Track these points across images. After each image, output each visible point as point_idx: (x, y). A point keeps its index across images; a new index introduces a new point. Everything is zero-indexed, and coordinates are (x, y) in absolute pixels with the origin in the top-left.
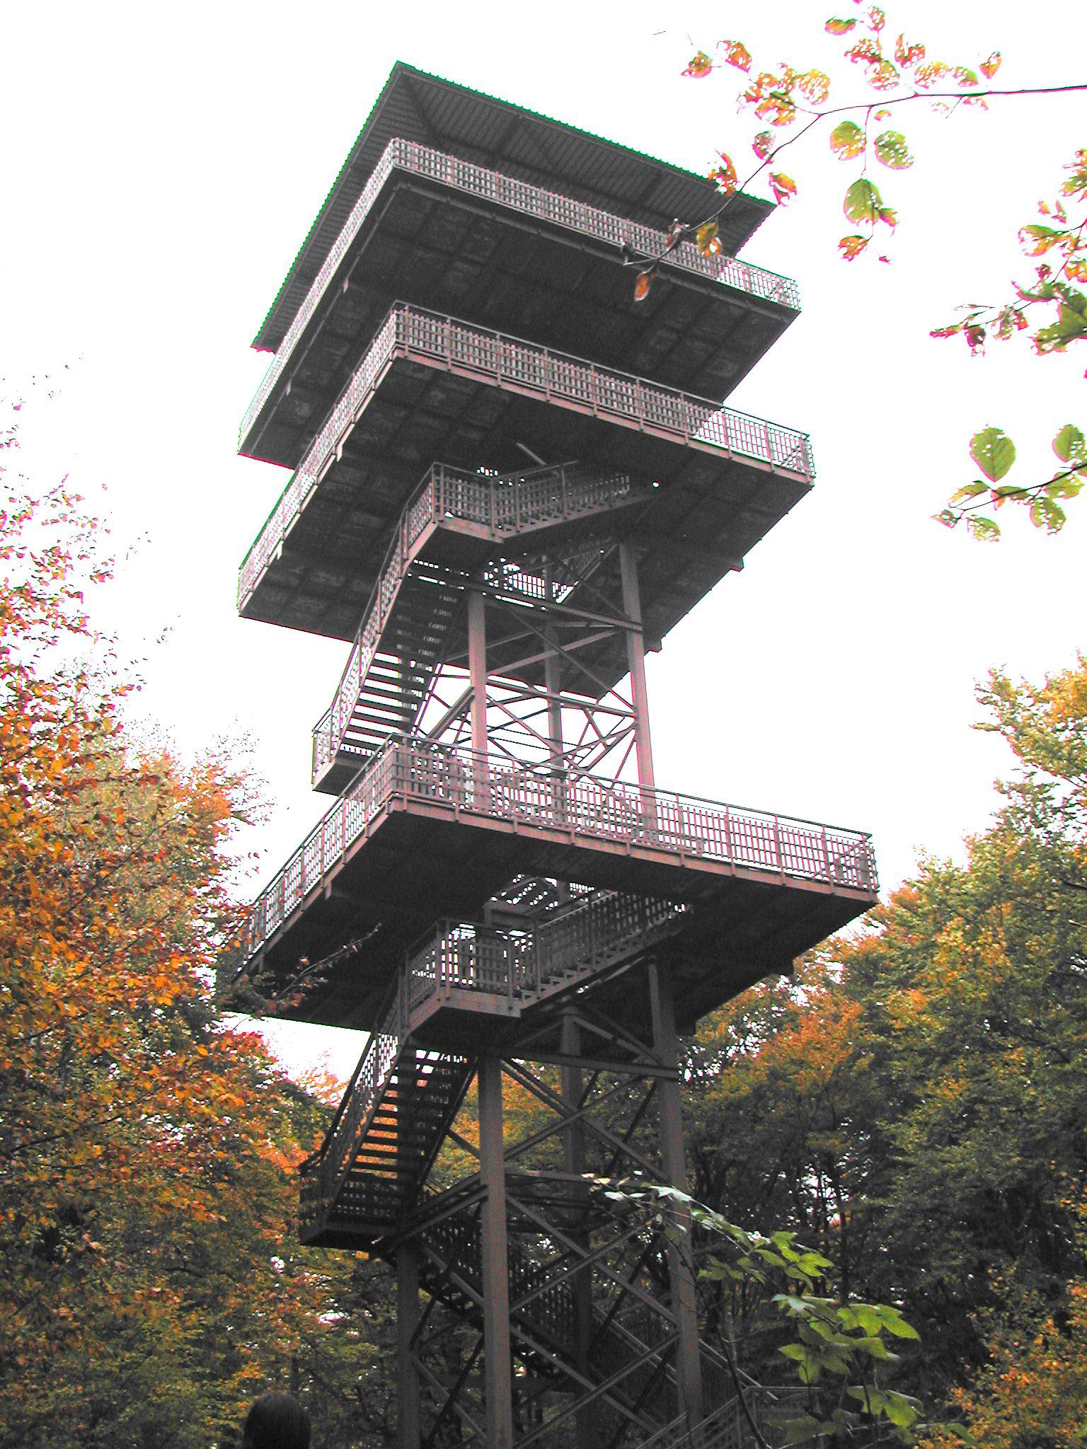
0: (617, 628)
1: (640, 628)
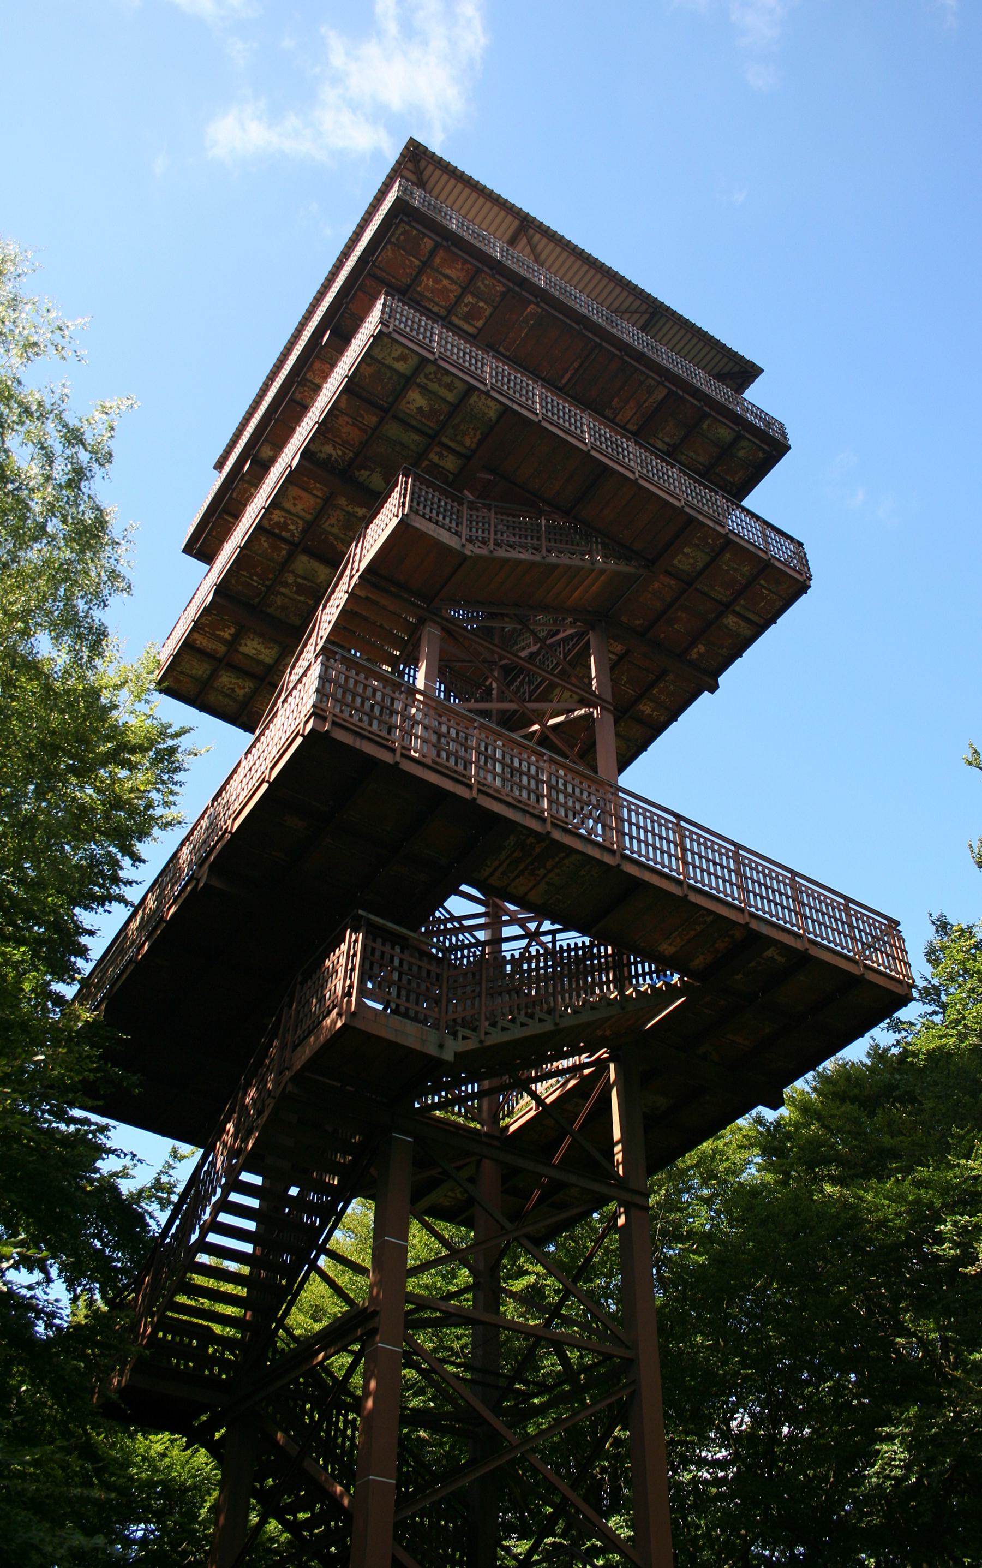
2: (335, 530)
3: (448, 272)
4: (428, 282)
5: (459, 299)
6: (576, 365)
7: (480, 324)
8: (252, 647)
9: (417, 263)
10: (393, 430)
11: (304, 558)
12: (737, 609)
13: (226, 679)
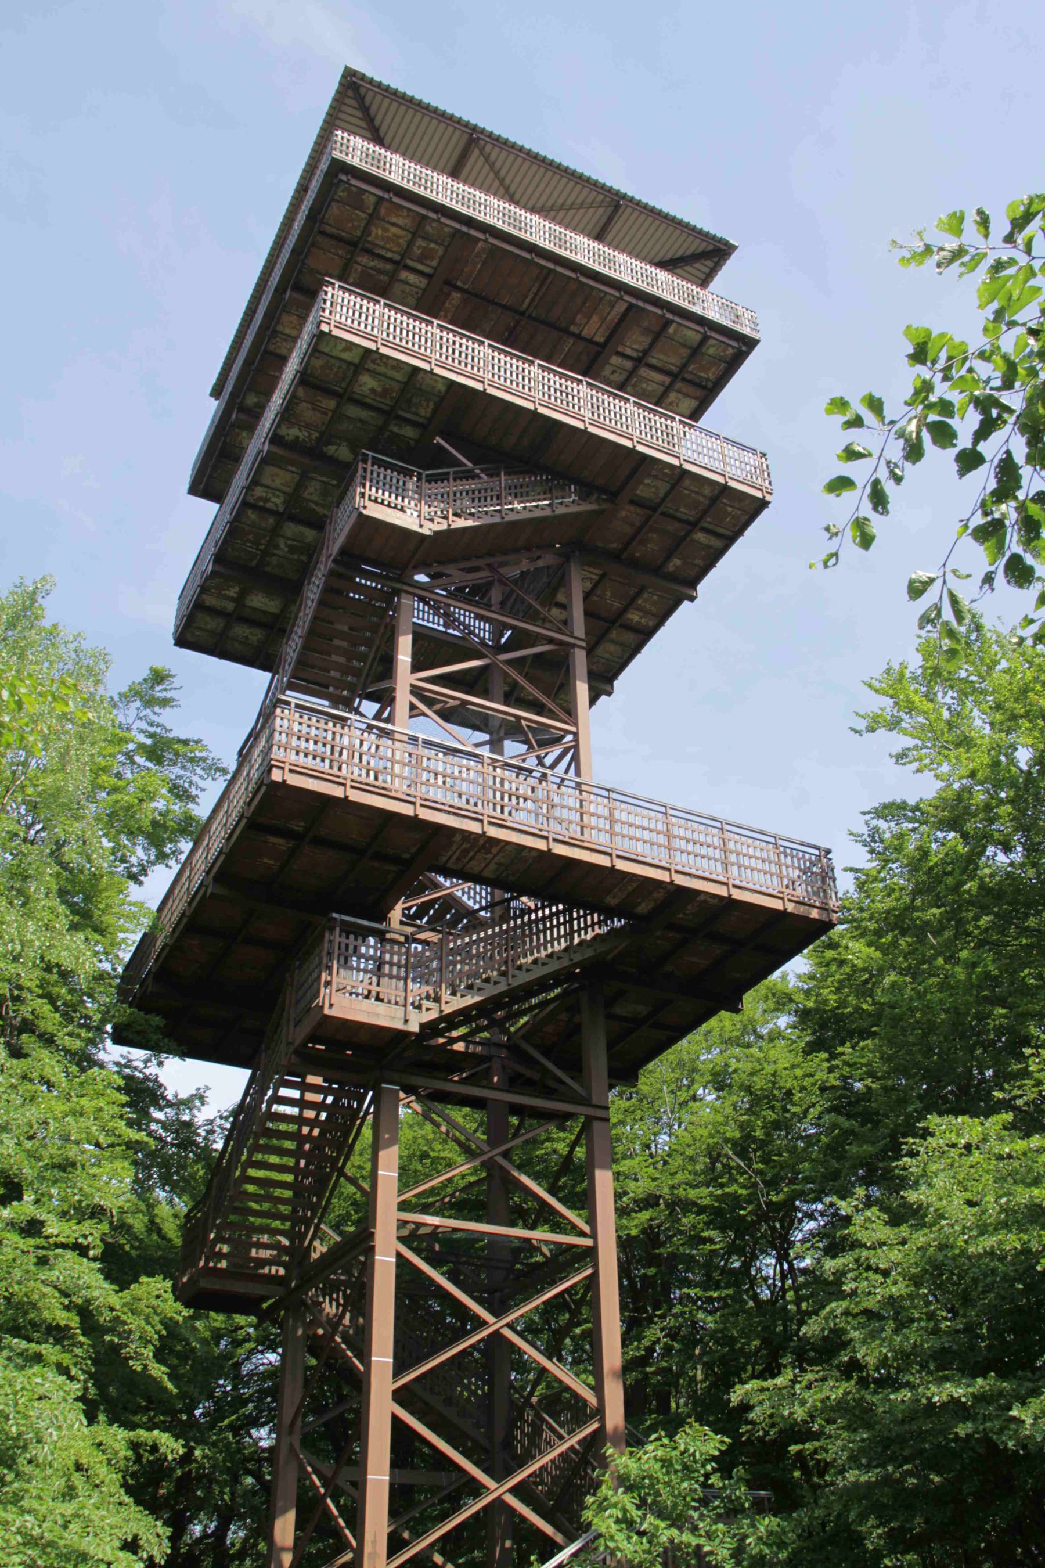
0: (561, 643)
1: (584, 644)
2: (315, 498)
3: (394, 220)
4: (377, 232)
5: (410, 244)
6: (534, 290)
7: (434, 263)
8: (260, 601)
9: (363, 215)
10: (353, 411)
11: (291, 525)
12: (705, 525)
13: (241, 631)
